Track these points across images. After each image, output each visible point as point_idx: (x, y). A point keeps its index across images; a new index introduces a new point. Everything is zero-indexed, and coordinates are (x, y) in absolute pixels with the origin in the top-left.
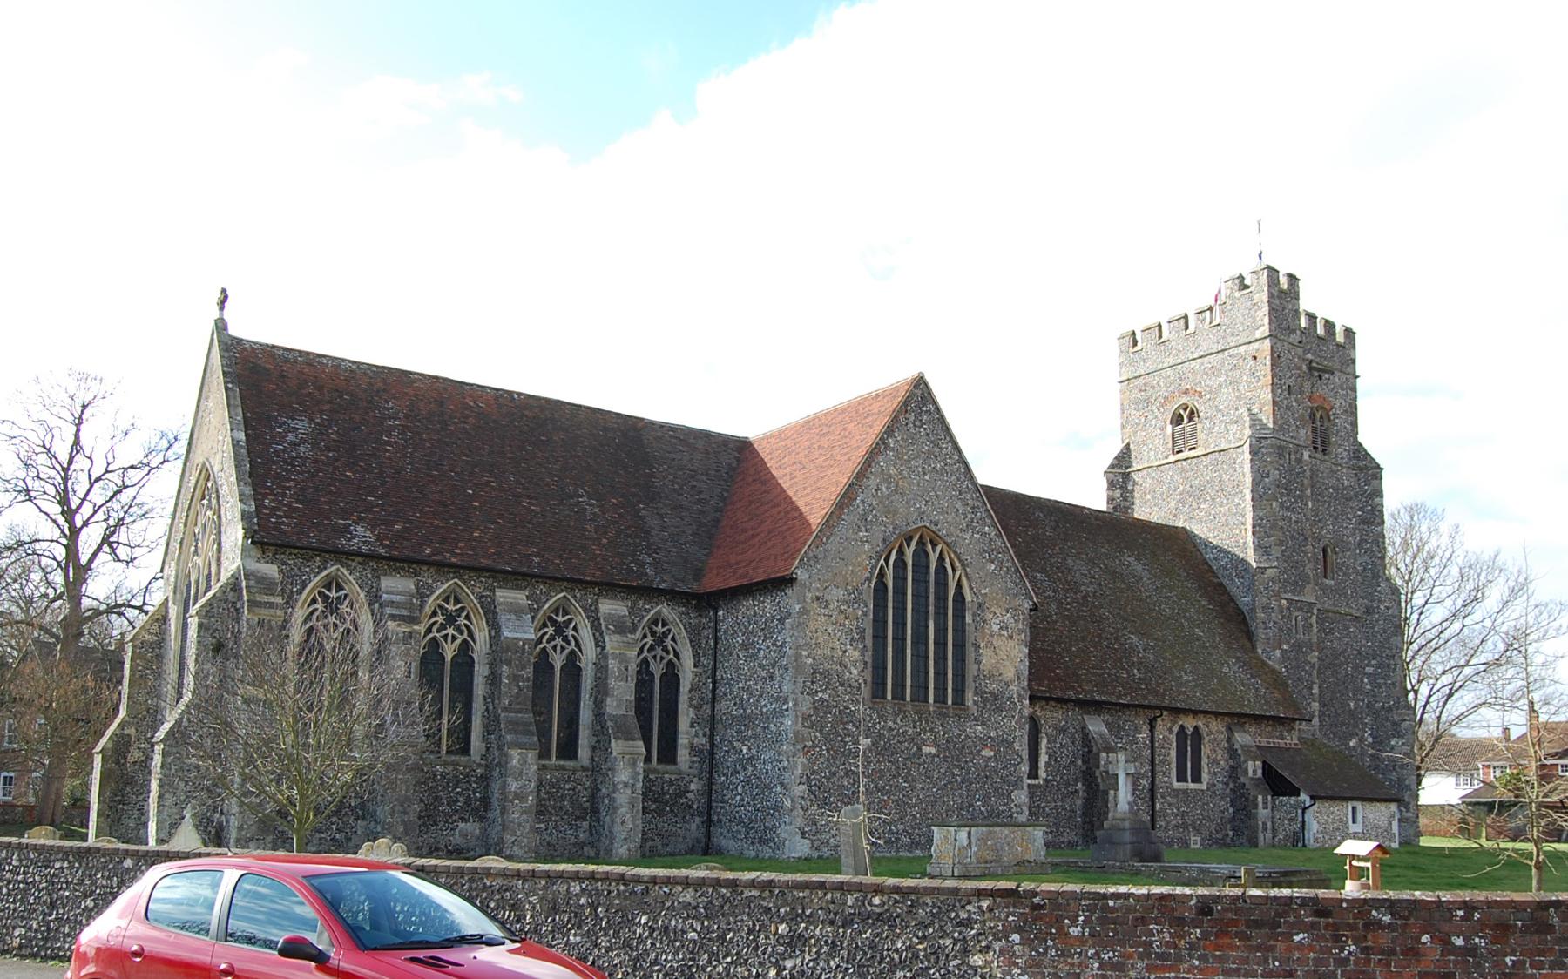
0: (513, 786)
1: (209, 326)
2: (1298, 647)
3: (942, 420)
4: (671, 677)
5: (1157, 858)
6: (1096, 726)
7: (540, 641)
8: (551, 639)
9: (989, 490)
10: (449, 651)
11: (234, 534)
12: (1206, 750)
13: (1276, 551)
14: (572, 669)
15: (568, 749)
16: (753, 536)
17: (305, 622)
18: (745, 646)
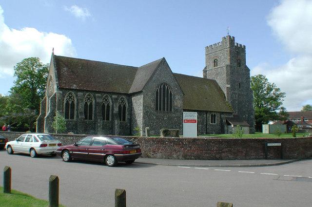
1: (51, 54)
2: (234, 100)
4: (124, 106)
9: (175, 75)
10: (89, 104)
11: (55, 87)
12: (216, 118)
14: (108, 106)
15: (108, 119)
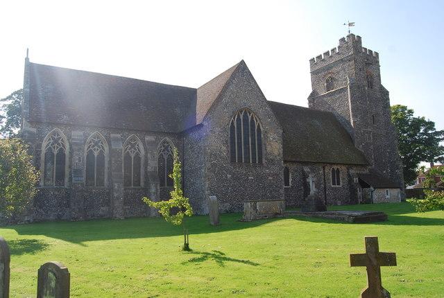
0: (116, 195)
2: (367, 144)
5: (324, 209)
6: (306, 169)
7: (126, 149)
8: (130, 149)
12: (341, 175)
13: (359, 116)
17: (47, 146)
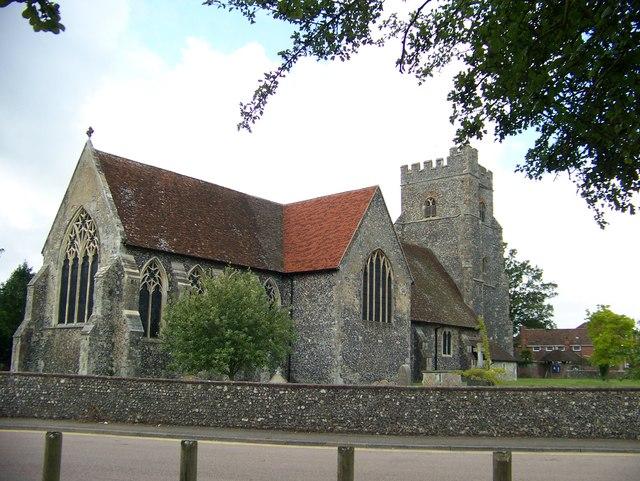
3: (385, 204)
16: (308, 250)
18: (309, 296)
